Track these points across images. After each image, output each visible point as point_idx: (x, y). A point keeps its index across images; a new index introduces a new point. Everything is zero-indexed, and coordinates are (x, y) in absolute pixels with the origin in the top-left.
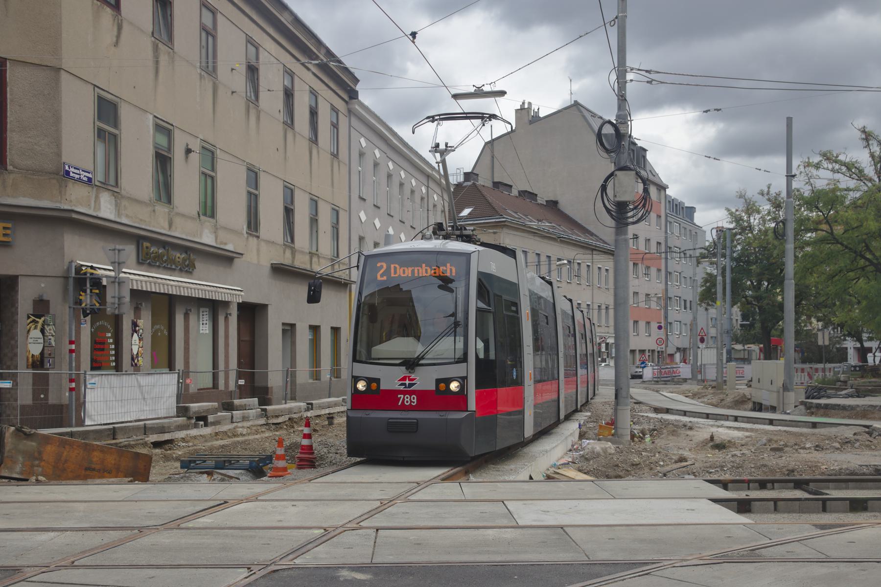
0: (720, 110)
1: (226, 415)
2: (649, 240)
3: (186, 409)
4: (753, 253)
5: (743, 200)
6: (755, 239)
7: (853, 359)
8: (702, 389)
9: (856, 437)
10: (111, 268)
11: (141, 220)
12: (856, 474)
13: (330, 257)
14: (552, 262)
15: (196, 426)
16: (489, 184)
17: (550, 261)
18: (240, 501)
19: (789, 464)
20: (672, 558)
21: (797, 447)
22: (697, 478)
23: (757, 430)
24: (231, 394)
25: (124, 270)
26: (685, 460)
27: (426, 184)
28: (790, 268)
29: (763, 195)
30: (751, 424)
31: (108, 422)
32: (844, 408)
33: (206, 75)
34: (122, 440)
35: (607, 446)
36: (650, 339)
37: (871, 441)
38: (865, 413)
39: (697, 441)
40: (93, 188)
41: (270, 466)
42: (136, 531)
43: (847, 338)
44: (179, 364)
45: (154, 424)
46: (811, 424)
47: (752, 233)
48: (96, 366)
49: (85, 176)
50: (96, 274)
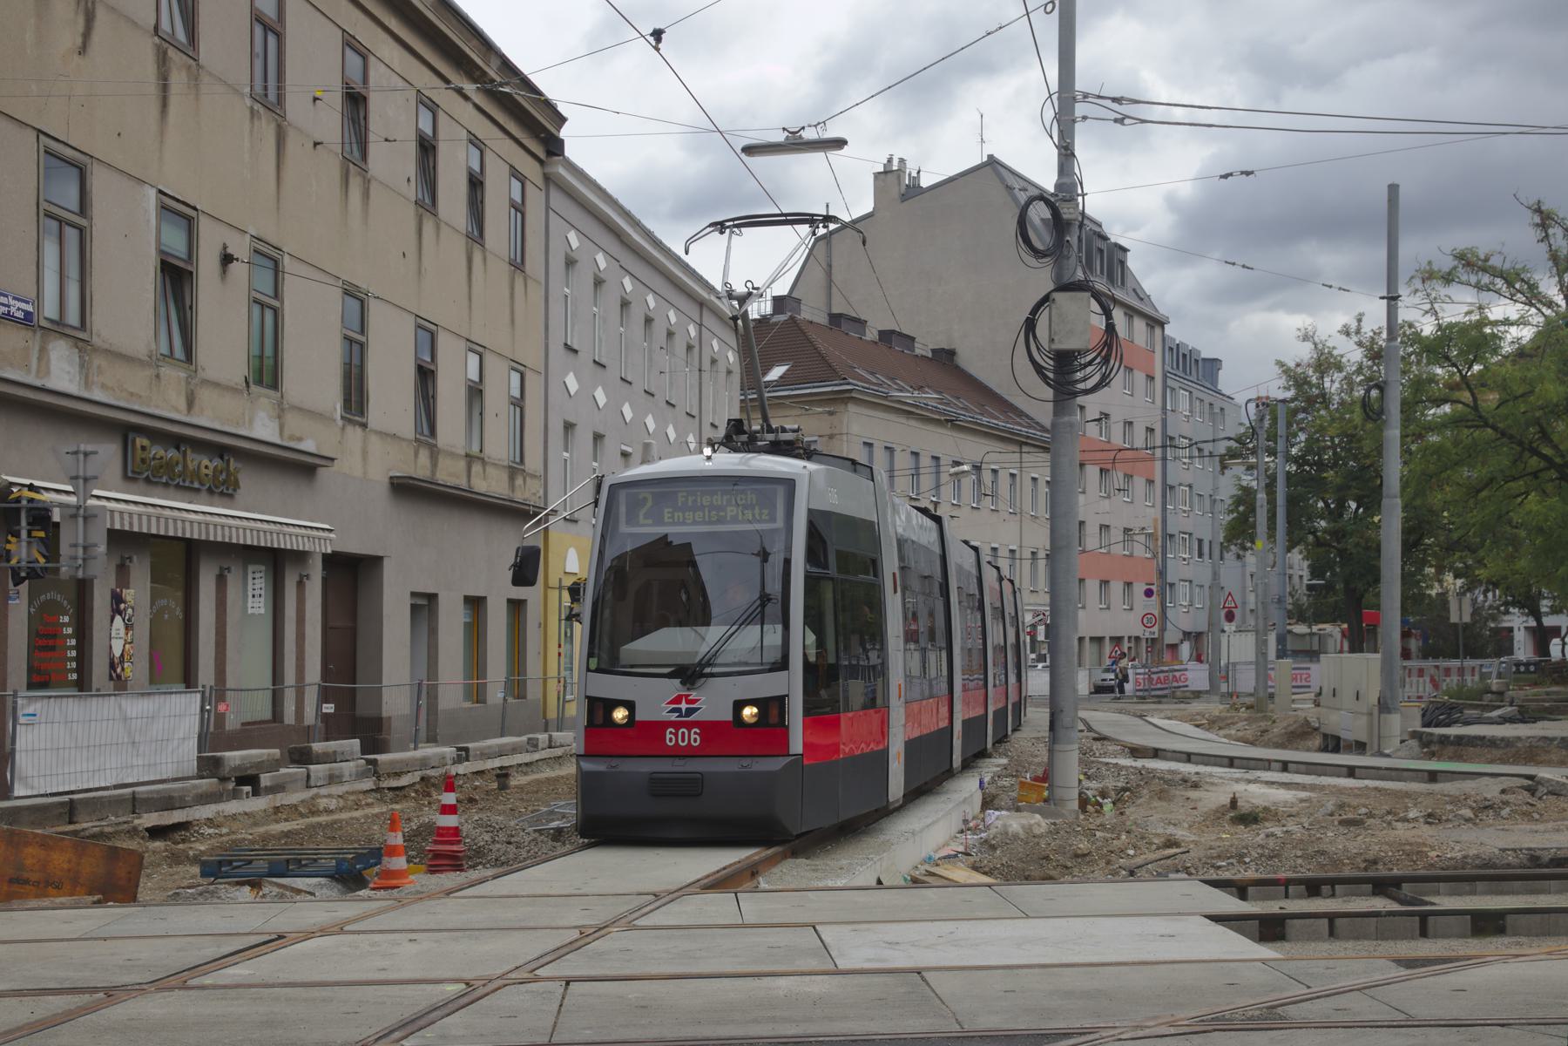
0: (1252, 173)
1: (296, 773)
2: (1131, 423)
3: (217, 762)
4: (1329, 447)
5: (1309, 346)
6: (1333, 420)
7: (1523, 649)
8: (1228, 711)
9: (1505, 797)
10: (70, 488)
11: (132, 394)
12: (1494, 866)
13: (506, 463)
14: (942, 469)
15: (235, 795)
16: (822, 319)
17: (938, 466)
18: (308, 935)
19: (1368, 849)
20: (1117, 1025)
21: (1390, 817)
22: (1193, 877)
23: (1322, 788)
24: (308, 733)
25: (95, 492)
26: (1176, 844)
27: (697, 318)
28: (1394, 470)
29: (1348, 334)
30: (1313, 777)
31: (61, 790)
32: (1492, 743)
33: (262, 110)
34: (86, 825)
35: (1032, 822)
36: (1131, 615)
37: (1532, 805)
38: (1532, 752)
39: (1206, 809)
40: (35, 332)
41: (377, 869)
42: (101, 995)
43: (1511, 610)
44: (206, 673)
45: (151, 792)
46: (1426, 774)
47: (1327, 408)
48: (40, 680)
49: (19, 309)
50: (39, 501)
